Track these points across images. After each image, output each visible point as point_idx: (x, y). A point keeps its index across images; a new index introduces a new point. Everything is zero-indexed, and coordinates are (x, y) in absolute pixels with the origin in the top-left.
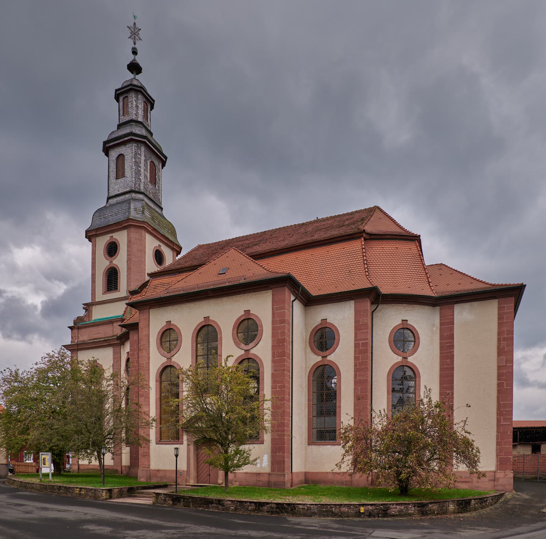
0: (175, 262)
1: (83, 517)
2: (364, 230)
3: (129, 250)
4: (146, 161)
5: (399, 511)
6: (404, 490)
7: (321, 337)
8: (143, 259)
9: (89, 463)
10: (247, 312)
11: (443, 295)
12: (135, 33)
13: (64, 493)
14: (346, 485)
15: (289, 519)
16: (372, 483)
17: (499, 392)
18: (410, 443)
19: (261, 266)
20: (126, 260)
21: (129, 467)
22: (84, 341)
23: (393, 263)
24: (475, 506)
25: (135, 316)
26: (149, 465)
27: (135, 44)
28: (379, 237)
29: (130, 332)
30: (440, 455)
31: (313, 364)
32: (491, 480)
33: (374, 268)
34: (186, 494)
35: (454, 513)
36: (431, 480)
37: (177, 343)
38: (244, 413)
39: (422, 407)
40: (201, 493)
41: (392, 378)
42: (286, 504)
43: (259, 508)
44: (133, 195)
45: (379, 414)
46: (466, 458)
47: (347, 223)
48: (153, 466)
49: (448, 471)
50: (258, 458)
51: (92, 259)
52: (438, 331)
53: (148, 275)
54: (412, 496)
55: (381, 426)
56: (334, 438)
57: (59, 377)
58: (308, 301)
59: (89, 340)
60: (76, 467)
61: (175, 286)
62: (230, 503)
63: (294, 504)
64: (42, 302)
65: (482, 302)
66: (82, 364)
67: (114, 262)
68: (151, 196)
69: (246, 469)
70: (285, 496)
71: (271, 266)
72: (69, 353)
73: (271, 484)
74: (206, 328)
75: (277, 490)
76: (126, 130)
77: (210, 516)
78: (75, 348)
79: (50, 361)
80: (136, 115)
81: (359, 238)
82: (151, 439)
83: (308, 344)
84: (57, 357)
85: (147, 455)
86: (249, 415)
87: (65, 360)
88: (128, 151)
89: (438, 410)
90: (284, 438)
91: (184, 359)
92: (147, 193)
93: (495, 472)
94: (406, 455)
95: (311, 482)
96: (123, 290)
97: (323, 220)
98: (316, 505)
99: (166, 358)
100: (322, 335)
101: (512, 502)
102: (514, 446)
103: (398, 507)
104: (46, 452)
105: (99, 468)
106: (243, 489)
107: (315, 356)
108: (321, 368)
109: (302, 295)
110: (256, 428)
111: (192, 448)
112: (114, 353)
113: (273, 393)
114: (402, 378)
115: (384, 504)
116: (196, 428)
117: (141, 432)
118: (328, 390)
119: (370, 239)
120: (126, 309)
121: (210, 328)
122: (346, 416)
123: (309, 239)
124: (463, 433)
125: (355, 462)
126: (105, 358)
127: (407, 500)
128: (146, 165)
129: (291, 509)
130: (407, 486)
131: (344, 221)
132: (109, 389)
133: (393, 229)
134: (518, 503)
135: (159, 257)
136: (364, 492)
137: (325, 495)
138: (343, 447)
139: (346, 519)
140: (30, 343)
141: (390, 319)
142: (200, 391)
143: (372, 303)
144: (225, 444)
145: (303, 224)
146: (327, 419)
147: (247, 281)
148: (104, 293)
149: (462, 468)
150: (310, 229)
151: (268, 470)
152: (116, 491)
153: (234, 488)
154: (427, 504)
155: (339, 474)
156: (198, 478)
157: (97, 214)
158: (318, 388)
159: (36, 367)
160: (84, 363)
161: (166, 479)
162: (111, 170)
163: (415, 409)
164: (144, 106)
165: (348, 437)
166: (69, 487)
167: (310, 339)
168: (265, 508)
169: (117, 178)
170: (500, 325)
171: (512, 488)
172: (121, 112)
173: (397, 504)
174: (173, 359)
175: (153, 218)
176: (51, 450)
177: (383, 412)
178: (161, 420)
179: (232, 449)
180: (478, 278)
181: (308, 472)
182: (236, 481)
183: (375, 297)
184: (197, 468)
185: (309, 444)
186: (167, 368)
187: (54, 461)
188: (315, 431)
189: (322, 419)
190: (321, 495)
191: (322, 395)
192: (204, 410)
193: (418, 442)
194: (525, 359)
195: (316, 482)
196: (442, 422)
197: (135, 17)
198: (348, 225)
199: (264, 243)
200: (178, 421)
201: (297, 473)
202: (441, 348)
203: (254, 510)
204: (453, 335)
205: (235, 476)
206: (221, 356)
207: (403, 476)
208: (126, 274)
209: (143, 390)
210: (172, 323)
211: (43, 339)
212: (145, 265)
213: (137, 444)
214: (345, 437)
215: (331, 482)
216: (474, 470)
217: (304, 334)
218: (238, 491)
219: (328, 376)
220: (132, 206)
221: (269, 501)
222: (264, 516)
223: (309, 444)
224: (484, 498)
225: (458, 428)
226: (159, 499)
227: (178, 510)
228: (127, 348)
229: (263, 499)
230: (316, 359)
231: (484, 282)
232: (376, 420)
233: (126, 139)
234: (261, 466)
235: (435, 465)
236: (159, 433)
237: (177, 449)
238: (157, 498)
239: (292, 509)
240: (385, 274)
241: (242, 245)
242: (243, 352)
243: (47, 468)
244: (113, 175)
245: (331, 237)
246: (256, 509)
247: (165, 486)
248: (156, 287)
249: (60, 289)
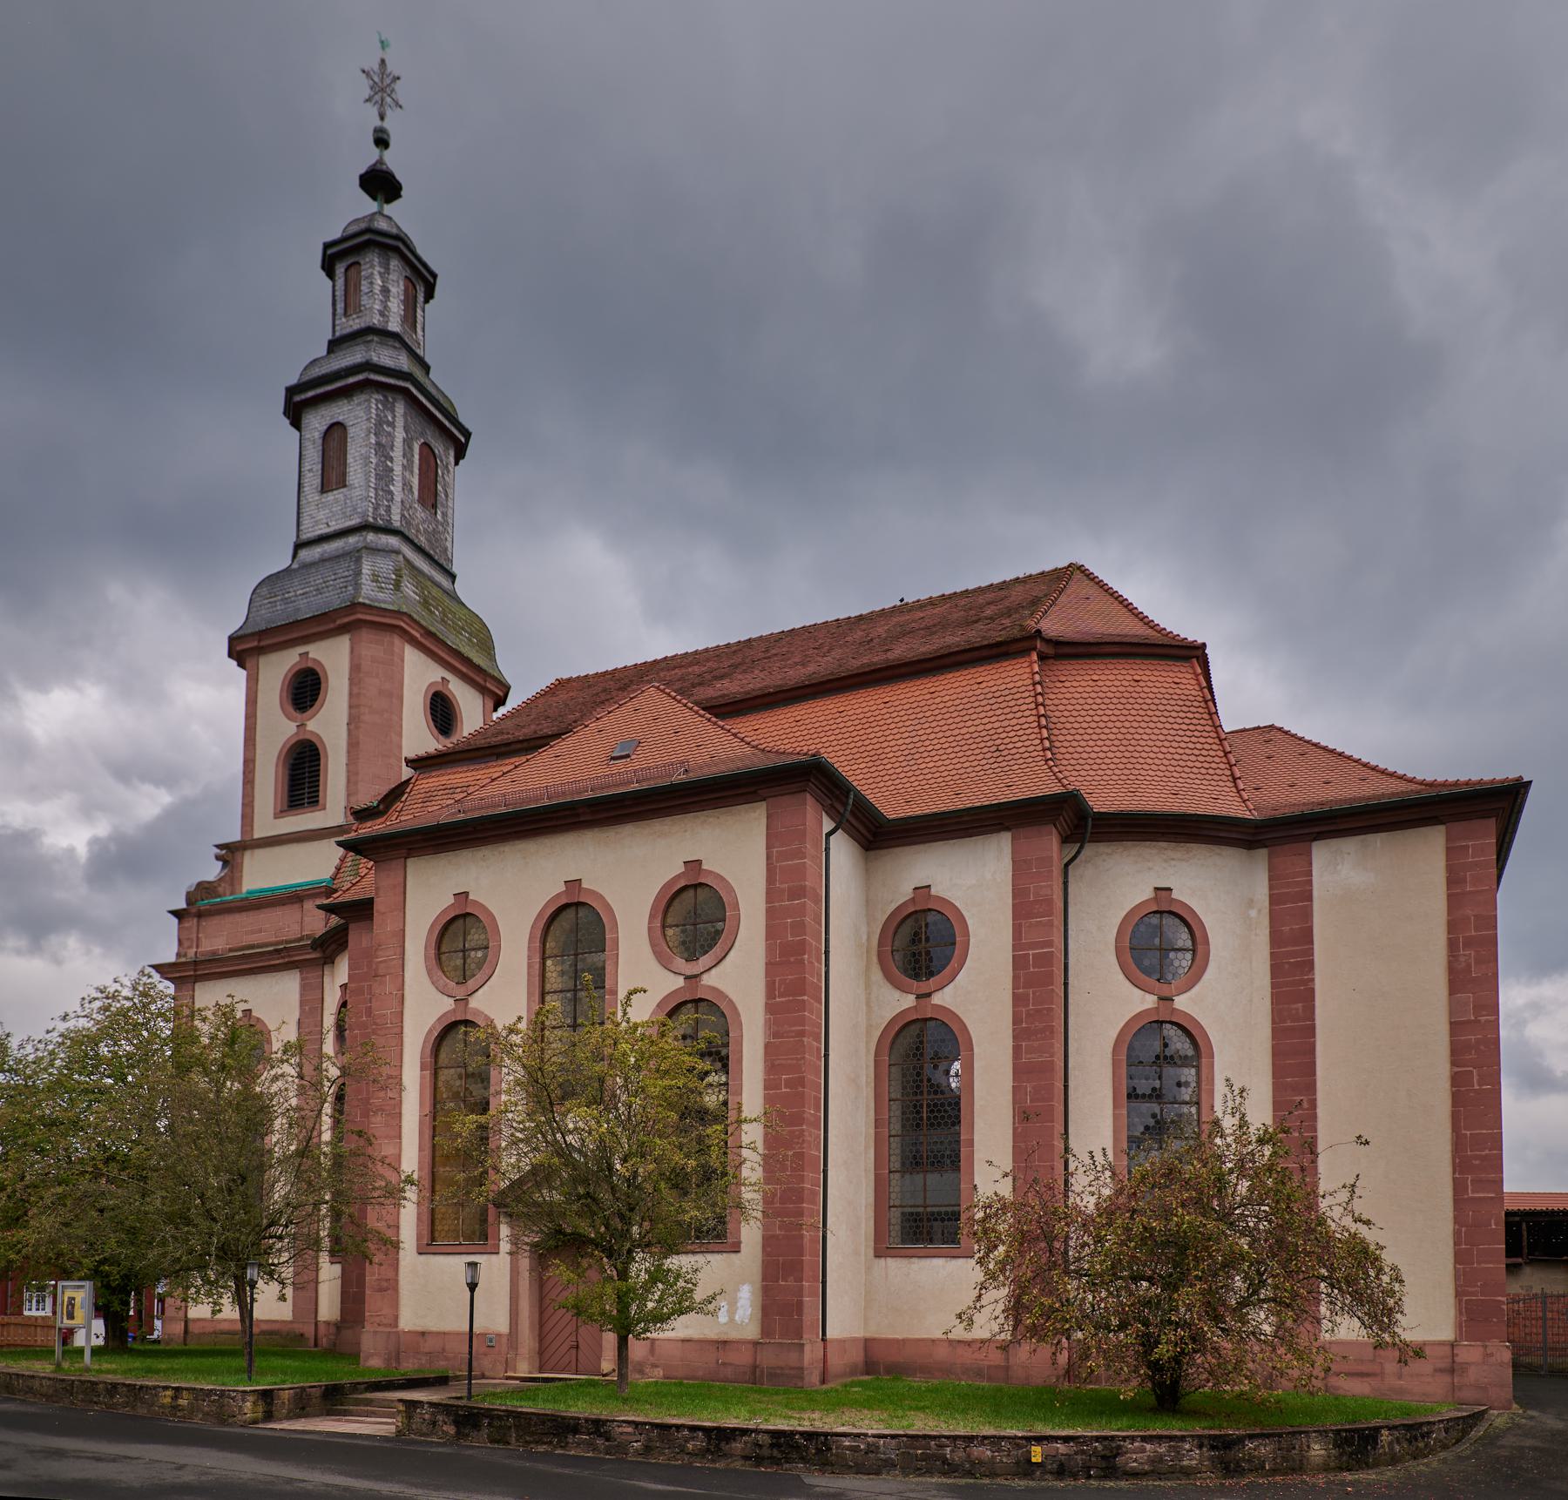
0: (488, 729)
1: (170, 1477)
2: (1039, 631)
3: (355, 690)
4: (408, 443)
5: (1151, 1461)
6: (1167, 1394)
7: (915, 938)
8: (395, 718)
9: (214, 1313)
10: (694, 865)
11: (1278, 814)
12: (382, 87)
13: (127, 1404)
14: (990, 1379)
15: (809, 1480)
16: (1069, 1373)
17: (1457, 1099)
18: (1183, 1250)
19: (735, 735)
20: (345, 721)
21: (339, 1326)
22: (214, 953)
23: (1127, 724)
24: (1391, 1449)
25: (365, 879)
26: (396, 1318)
27: (382, 118)
28: (1081, 650)
29: (351, 926)
30: (1276, 1287)
31: (889, 1015)
32: (1441, 1371)
33: (1069, 738)
34: (497, 1404)
35: (1326, 1468)
36: (1251, 1365)
37: (485, 956)
38: (678, 1158)
39: (1218, 1141)
40: (546, 1401)
41: (1129, 1056)
42: (802, 1434)
43: (717, 1446)
44: (371, 537)
45: (1088, 1161)
46: (1358, 1297)
47: (988, 612)
48: (409, 1320)
49: (1303, 1341)
50: (723, 1295)
51: (247, 718)
52: (1266, 922)
53: (409, 762)
54: (1194, 1414)
55: (1093, 1200)
56: (952, 1238)
57: (129, 1056)
58: (874, 835)
59: (231, 950)
60: (178, 1328)
61: (483, 793)
62: (630, 1430)
63: (826, 1435)
64: (94, 842)
65: (1399, 835)
66: (204, 1020)
67: (311, 726)
68: (422, 540)
69: (683, 1327)
70: (803, 1410)
71: (766, 738)
72: (168, 988)
73: (761, 1373)
74: (570, 914)
75: (777, 1393)
76: (353, 356)
77: (567, 1471)
78: (186, 973)
79: (106, 1009)
80: (382, 314)
81: (1024, 652)
82: (402, 1238)
83: (875, 959)
84: (127, 998)
85: (390, 1287)
86: (692, 1163)
87: (153, 1007)
88: (357, 415)
89: (1268, 1150)
90: (802, 1236)
91: (505, 1000)
92: (411, 533)
93: (1452, 1345)
94: (1171, 1286)
95: (884, 1368)
96: (333, 810)
97: (920, 605)
98: (893, 1437)
99: (451, 1001)
100: (916, 934)
101: (1509, 1440)
102: (1512, 1269)
103: (1148, 1447)
104: (80, 1279)
105: (238, 1327)
106: (674, 1390)
107: (897, 994)
108: (914, 1030)
109: (857, 818)
110: (714, 1205)
111: (525, 1263)
112: (304, 988)
113: (769, 1100)
114: (1158, 1057)
115: (1105, 1438)
116: (536, 1204)
117: (374, 1220)
118: (936, 1093)
119: (1058, 657)
120: (342, 860)
121: (582, 912)
122: (990, 1168)
123: (877, 658)
124: (1348, 1221)
125: (1016, 1309)
126: (274, 1002)
127: (1175, 1427)
128: (408, 455)
129: (816, 1449)
130: (1176, 1382)
131: (981, 608)
132: (274, 1088)
133: (1129, 629)
134: (1529, 1442)
135: (442, 712)
136: (1042, 1400)
137: (923, 1409)
138: (980, 1262)
139: (987, 1481)
140: (58, 961)
141: (1118, 885)
142: (547, 1094)
143: (1065, 840)
144: (617, 1251)
145: (860, 618)
146: (933, 1179)
147: (693, 776)
148: (279, 814)
149: (1348, 1329)
150: (881, 630)
151: (752, 1331)
152: (286, 1395)
153: (648, 1385)
154: (1240, 1440)
155: (969, 1343)
156: (542, 1356)
157: (264, 591)
158: (904, 1088)
159: (62, 1027)
160: (209, 1014)
161: (447, 1359)
162: (307, 467)
163: (1198, 1146)
164: (406, 290)
165: (994, 1231)
166: (141, 1387)
167: (880, 944)
168: (738, 1446)
169: (325, 488)
170: (1454, 901)
171: (1510, 1396)
172: (340, 306)
173: (1144, 1439)
174: (474, 1003)
175: (425, 603)
176: (95, 1274)
177: (1099, 1158)
178: (434, 1180)
179: (640, 1267)
180: (1382, 766)
182: (655, 1366)
183: (1073, 823)
184: (541, 1326)
185: (878, 1255)
186: (449, 1030)
187: (100, 1310)
188: (895, 1215)
189: (919, 1178)
190: (911, 1409)
191: (917, 1109)
192: (563, 1152)
193: (1207, 1248)
194: (1537, 1008)
195: (897, 1370)
196: (1280, 1187)
197: (383, 44)
198: (992, 619)
199: (745, 672)
200: (480, 1181)
201: (842, 1342)
202: (1276, 969)
203: (702, 1453)
204: (1310, 929)
205: (652, 1350)
206: (614, 993)
207: (1163, 1351)
208: (343, 759)
209: (382, 1094)
210: (471, 897)
211: (97, 950)
212: (400, 735)
213: (361, 1252)
214: (985, 1232)
215: (946, 1370)
216: (1386, 1336)
217: (864, 929)
218: (658, 1394)
219: (936, 1053)
220: (366, 569)
221: (751, 1425)
222: (736, 1471)
223: (878, 1255)
224: (1422, 1424)
225: (1331, 1207)
226: (417, 1419)
227: (470, 1452)
228: (341, 972)
229: (733, 1419)
230: (898, 1002)
231: (1402, 777)
232: (1079, 1182)
233: (351, 380)
234: (732, 1320)
235: (1263, 1320)
236: (426, 1217)
237: (473, 1265)
238: (409, 1418)
239: (819, 1451)
240: (1102, 755)
241: (681, 679)
242: (680, 982)
243: (91, 1333)
244: (313, 480)
245: (943, 652)
246: (708, 1450)
247: (442, 1381)
248: (428, 798)
249: (150, 803)
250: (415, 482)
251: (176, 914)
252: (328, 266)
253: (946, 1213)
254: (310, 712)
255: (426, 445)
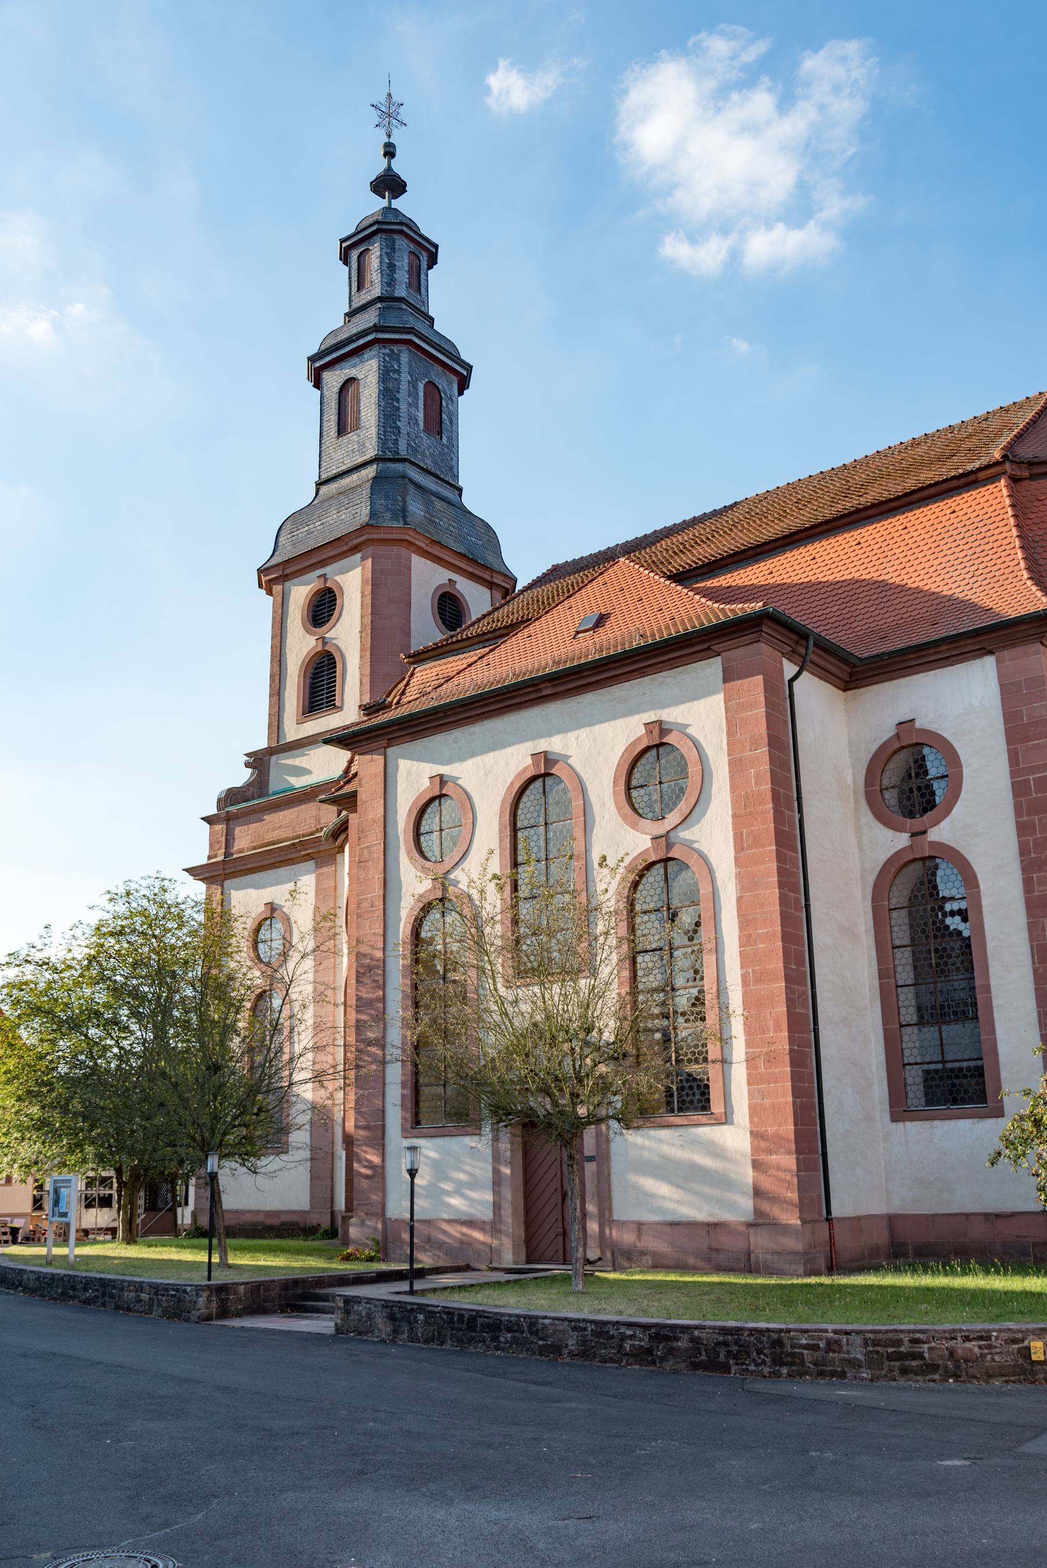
4: (413, 384)
26: (383, 1206)
27: (389, 136)
37: (460, 832)
68: (428, 464)
81: (993, 479)
107: (889, 833)
135: (449, 608)
146: (951, 1031)
172: (355, 285)
181: (898, 1216)
188: (914, 1077)
197: (390, 152)
230: (893, 841)
233: (361, 342)
250: (421, 415)
251: (209, 820)
252: (345, 259)
253: (969, 1069)
254: (328, 625)
255: (431, 386)
